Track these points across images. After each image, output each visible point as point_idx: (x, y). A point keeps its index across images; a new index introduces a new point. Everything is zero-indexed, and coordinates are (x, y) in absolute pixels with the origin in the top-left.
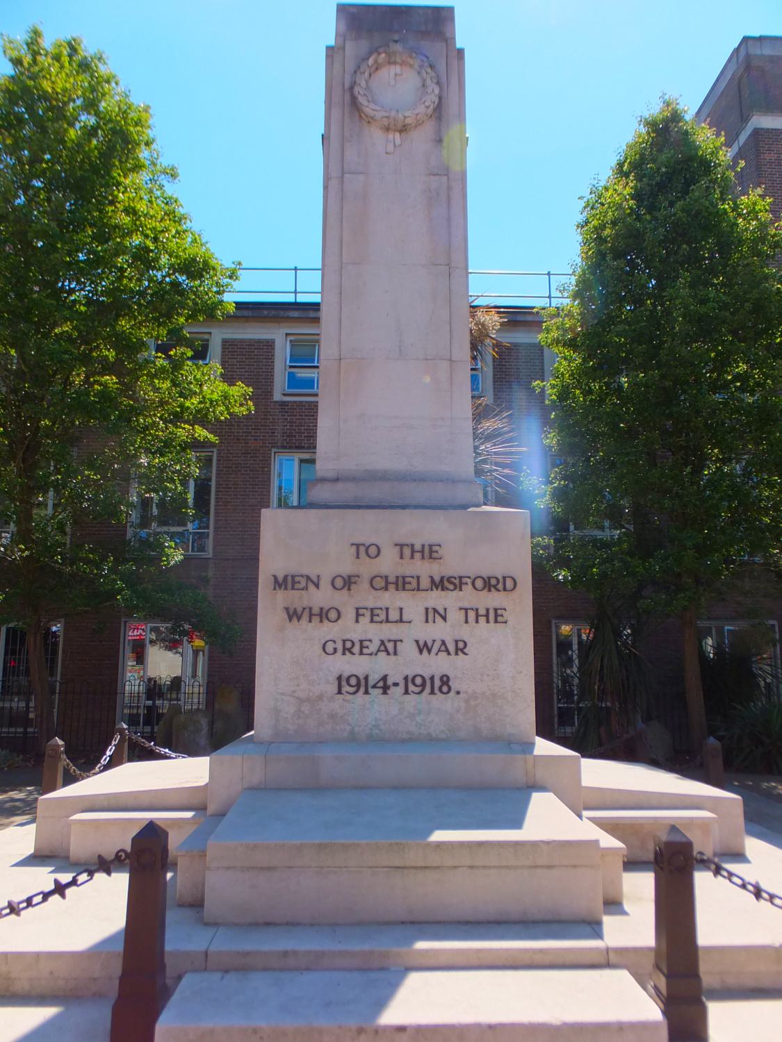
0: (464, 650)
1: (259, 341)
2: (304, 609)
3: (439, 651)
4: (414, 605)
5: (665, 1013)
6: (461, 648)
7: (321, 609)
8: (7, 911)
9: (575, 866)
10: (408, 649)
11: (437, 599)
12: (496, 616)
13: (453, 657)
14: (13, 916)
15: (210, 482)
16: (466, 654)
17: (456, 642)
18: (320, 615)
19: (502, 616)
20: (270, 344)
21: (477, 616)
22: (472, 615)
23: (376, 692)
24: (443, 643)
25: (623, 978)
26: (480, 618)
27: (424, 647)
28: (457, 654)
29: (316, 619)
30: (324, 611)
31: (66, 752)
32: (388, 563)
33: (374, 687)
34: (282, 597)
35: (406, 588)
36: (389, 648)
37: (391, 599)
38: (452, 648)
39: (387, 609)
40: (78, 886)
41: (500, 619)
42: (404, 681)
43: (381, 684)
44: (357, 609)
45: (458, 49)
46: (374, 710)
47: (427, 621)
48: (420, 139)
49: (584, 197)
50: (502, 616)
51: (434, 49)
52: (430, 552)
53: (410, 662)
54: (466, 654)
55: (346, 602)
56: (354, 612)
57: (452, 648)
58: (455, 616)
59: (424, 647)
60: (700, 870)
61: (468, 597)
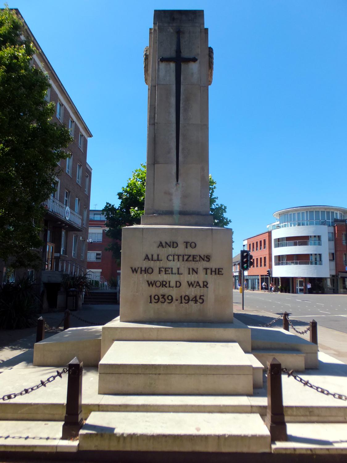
0: (166, 285)
2: (138, 268)
3: (196, 286)
5: (271, 431)
6: (205, 285)
7: (145, 268)
8: (41, 385)
9: (232, 375)
13: (202, 288)
14: (27, 388)
16: (207, 287)
17: (204, 282)
18: (145, 271)
19: (221, 272)
21: (211, 271)
22: (209, 271)
23: (191, 303)
24: (198, 282)
25: (257, 417)
26: (142, 272)
27: (190, 284)
28: (203, 287)
29: (143, 272)
30: (147, 269)
31: (104, 324)
33: (192, 300)
35: (194, 260)
38: (202, 285)
39: (172, 269)
40: (52, 376)
41: (220, 273)
42: (180, 298)
43: (194, 299)
44: (160, 268)
45: (205, 29)
47: (189, 274)
50: (221, 272)
54: (207, 287)
56: (158, 269)
57: (202, 285)
59: (190, 284)
60: (283, 374)
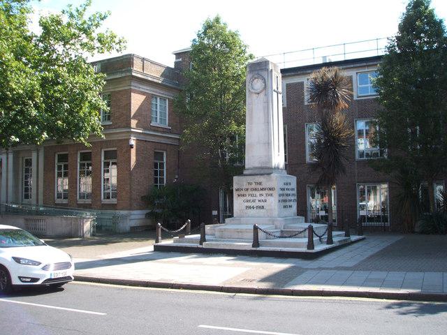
1: (299, 83)
4: (257, 193)
10: (257, 201)
11: (261, 192)
12: (271, 195)
15: (31, 165)
20: (302, 84)
27: (259, 201)
32: (254, 186)
34: (238, 193)
36: (254, 201)
37: (254, 192)
46: (252, 212)
48: (262, 95)
49: (40, 263)
51: (264, 74)
52: (260, 184)
53: (258, 204)
55: (247, 193)
58: (265, 195)
59: (259, 201)
61: (267, 192)
